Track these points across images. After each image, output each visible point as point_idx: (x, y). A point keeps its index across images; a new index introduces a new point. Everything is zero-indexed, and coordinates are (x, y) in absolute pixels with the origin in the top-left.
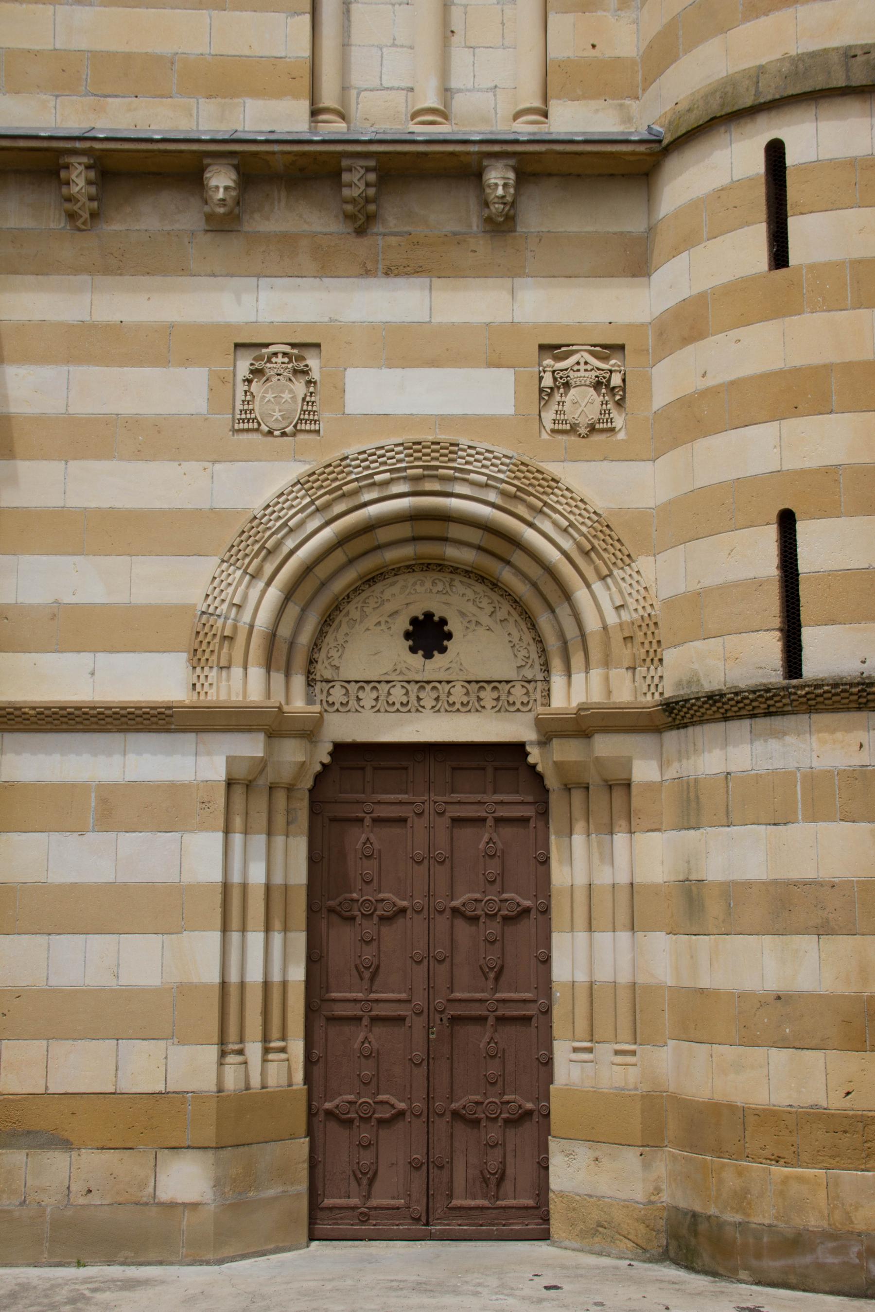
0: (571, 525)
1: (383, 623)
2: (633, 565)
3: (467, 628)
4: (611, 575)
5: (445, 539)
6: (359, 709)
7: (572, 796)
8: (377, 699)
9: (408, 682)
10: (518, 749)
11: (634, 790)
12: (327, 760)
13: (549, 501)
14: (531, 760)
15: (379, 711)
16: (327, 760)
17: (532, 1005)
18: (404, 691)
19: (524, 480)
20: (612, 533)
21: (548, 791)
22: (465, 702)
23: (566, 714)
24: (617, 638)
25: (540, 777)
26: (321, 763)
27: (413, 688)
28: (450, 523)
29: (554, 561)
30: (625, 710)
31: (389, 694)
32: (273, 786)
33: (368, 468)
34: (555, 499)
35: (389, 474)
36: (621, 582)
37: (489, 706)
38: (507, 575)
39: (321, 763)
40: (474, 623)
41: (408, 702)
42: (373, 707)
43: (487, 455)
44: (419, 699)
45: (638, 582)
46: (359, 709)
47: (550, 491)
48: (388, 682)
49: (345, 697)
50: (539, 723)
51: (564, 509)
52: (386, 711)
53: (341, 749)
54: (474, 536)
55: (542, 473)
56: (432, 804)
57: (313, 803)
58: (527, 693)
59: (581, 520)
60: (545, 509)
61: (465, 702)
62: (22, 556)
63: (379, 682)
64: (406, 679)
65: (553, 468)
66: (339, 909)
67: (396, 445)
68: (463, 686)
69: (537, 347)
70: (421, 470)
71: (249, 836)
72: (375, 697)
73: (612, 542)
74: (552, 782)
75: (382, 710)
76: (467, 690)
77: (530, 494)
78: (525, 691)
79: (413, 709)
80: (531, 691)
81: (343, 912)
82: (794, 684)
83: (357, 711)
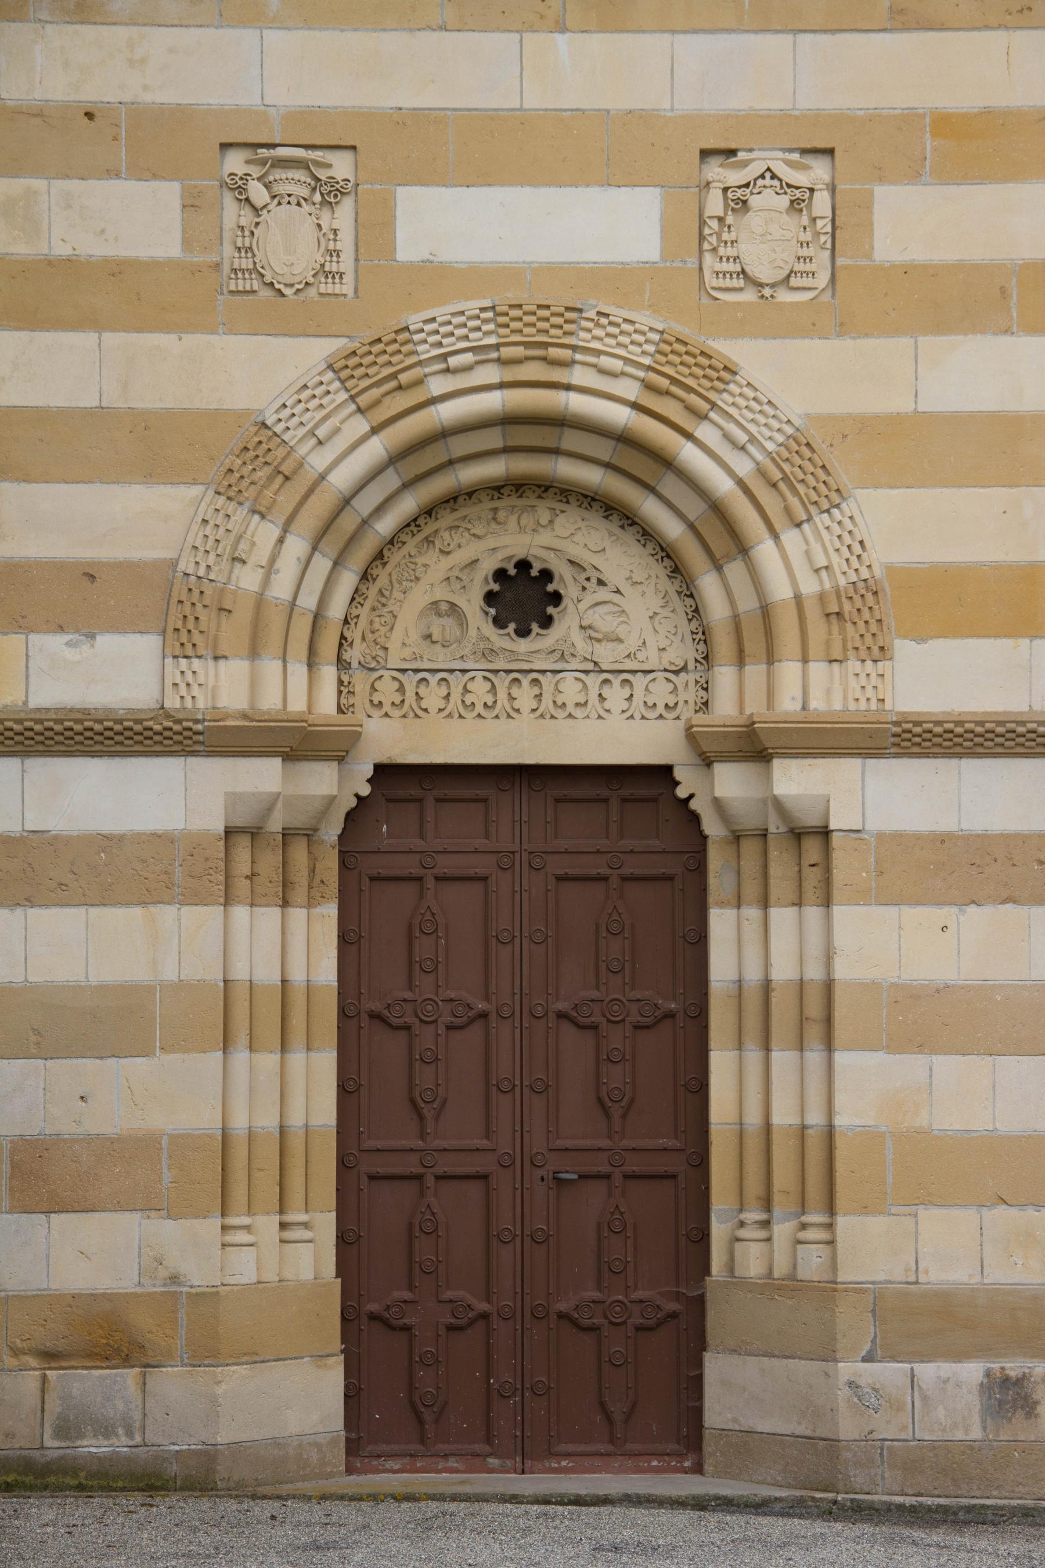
0: (753, 439)
1: (452, 579)
2: (844, 506)
3: (584, 588)
4: (809, 519)
5: (556, 452)
6: (420, 713)
7: (741, 845)
8: (447, 697)
9: (496, 672)
10: (664, 773)
11: (836, 839)
12: (365, 790)
13: (720, 403)
14: (682, 792)
15: (632, 717)
16: (365, 790)
17: (1009, 729)
18: (396, 685)
19: (680, 368)
20: (829, 480)
21: (705, 838)
22: (671, 705)
23: (785, 722)
24: (813, 614)
25: (695, 818)
26: (357, 796)
27: (502, 682)
28: (566, 429)
29: (718, 495)
30: (781, 725)
31: (466, 690)
32: (286, 832)
33: (440, 344)
34: (730, 400)
35: (470, 354)
36: (824, 533)
37: (433, 710)
38: (651, 509)
39: (357, 796)
40: (594, 581)
41: (403, 701)
42: (534, 710)
43: (625, 327)
44: (512, 698)
45: (850, 532)
46: (420, 713)
47: (721, 386)
48: (464, 671)
49: (397, 694)
50: (691, 736)
51: (759, 432)
52: (643, 718)
53: (384, 773)
54: (694, 508)
55: (710, 357)
56: (525, 855)
57: (344, 856)
58: (675, 690)
59: (768, 433)
60: (782, 486)
61: (671, 705)
62: (1020, 710)
63: (451, 671)
64: (491, 666)
65: (726, 348)
66: (386, 1013)
67: (483, 310)
68: (485, 678)
69: (698, 151)
70: (522, 348)
71: (229, 908)
72: (628, 696)
73: (827, 493)
74: (711, 827)
75: (637, 716)
76: (493, 683)
77: (690, 389)
78: (671, 686)
79: (637, 716)
80: (680, 688)
81: (391, 1018)
82: (9, 1169)
83: (600, 717)
